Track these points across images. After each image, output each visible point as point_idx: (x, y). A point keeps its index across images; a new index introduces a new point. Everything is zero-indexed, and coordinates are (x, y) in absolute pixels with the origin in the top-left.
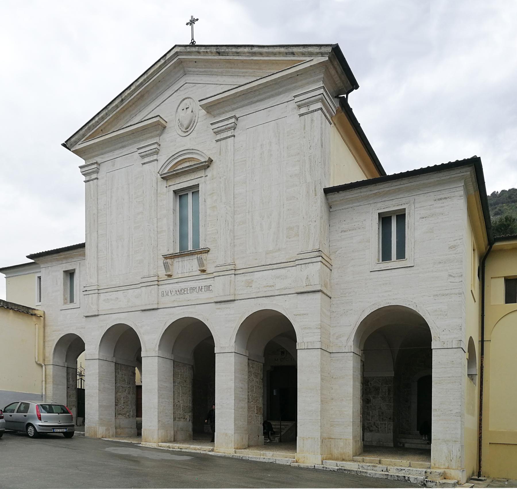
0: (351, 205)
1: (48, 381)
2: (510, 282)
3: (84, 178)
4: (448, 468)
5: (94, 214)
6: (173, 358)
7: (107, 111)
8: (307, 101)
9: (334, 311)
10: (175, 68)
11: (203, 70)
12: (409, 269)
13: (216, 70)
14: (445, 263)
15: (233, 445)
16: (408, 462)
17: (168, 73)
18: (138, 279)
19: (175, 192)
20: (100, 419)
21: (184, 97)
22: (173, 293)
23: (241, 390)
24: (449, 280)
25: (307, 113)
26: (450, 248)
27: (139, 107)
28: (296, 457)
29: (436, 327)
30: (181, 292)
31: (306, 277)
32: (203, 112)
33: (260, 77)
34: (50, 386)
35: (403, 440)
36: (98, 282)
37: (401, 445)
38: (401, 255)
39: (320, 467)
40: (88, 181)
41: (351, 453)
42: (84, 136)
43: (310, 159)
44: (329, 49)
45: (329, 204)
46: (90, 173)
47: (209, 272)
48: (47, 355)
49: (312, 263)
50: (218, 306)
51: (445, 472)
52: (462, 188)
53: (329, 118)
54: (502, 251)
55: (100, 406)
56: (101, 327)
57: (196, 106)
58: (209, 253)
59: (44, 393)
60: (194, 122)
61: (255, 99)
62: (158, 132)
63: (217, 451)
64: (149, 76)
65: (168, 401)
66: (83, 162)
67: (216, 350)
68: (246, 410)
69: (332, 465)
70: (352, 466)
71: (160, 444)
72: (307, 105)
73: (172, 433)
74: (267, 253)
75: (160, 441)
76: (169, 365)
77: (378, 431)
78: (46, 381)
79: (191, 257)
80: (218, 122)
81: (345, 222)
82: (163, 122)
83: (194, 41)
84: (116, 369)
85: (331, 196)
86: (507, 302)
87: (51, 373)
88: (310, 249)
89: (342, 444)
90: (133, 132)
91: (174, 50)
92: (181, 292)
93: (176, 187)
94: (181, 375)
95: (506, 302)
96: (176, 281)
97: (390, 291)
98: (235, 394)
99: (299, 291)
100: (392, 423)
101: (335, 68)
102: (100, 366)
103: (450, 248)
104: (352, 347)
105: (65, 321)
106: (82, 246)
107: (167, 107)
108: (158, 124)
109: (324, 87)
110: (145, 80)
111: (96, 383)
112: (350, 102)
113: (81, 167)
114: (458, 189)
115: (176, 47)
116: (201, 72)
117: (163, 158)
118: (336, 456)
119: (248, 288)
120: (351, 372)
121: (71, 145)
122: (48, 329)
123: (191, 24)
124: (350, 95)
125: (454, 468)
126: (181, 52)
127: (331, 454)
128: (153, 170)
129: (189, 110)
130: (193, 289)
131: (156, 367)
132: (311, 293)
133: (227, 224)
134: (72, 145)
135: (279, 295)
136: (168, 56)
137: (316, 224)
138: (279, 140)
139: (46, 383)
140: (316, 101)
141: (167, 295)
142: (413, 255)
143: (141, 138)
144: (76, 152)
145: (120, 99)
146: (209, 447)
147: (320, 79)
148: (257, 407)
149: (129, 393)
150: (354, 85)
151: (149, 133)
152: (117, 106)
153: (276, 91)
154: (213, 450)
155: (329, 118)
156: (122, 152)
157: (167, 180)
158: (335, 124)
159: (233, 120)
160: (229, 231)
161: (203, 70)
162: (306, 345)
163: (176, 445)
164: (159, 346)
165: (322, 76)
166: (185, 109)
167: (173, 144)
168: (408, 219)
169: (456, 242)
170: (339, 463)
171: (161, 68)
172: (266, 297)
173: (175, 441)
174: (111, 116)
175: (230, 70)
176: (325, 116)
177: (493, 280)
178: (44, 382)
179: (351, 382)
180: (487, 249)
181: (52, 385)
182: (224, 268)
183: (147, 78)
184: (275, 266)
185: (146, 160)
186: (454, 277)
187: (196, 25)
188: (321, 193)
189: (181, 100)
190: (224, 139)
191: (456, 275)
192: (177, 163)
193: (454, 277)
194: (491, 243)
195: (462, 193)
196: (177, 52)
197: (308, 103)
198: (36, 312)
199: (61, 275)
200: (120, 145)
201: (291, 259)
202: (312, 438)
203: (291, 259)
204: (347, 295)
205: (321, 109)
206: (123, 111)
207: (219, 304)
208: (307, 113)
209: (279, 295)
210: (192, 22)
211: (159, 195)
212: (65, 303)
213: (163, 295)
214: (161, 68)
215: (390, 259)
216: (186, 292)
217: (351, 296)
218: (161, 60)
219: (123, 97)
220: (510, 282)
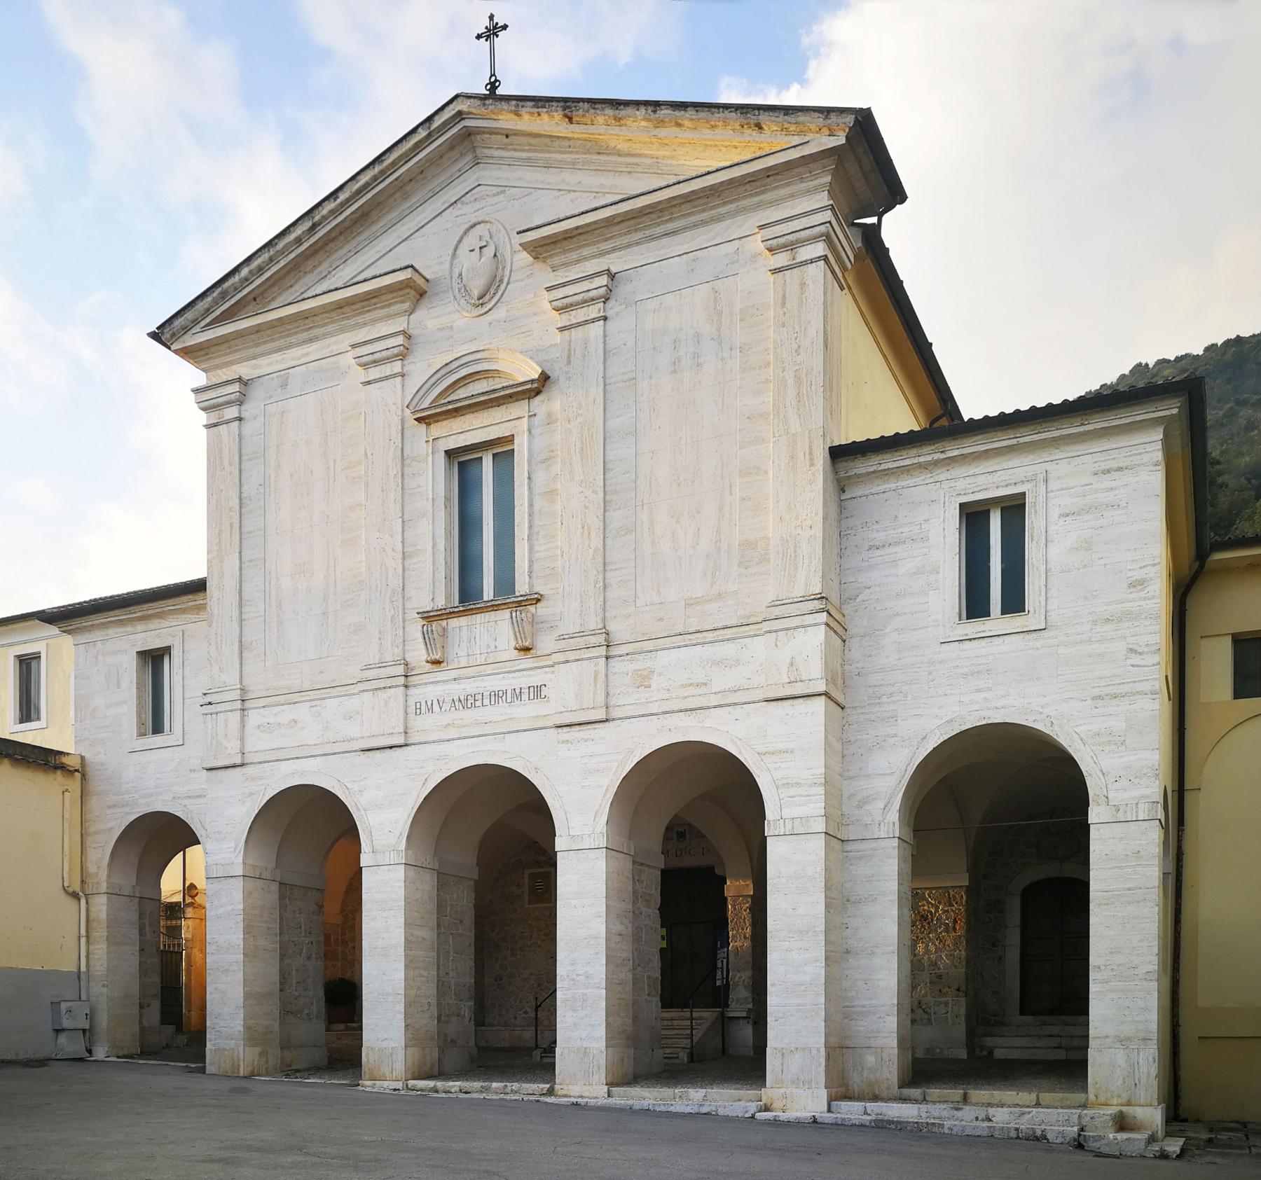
0: (893, 486)
1: (95, 934)
2: (1242, 643)
3: (203, 418)
4: (1129, 1104)
5: (231, 509)
6: (437, 867)
7: (272, 252)
8: (790, 237)
9: (853, 739)
10: (452, 148)
11: (525, 155)
12: (1034, 635)
13: (559, 156)
14: (1119, 621)
15: (603, 1075)
16: (1034, 1096)
17: (435, 161)
18: (354, 672)
19: (449, 453)
20: (247, 1028)
21: (474, 221)
22: (446, 707)
23: (619, 939)
24: (1130, 662)
25: (789, 268)
26: (1131, 585)
27: (354, 242)
28: (764, 1098)
29: (1100, 774)
30: (466, 702)
31: (788, 662)
32: (525, 257)
33: (674, 179)
34: (101, 949)
35: (989, 1041)
36: (241, 682)
37: (985, 1053)
38: (1014, 602)
39: (828, 1118)
40: (215, 425)
41: (896, 1080)
42: (208, 311)
43: (798, 379)
44: (850, 120)
45: (839, 481)
46: (224, 405)
47: (539, 653)
48: (92, 869)
49: (803, 627)
50: (565, 734)
51: (1121, 1112)
52: (1159, 446)
53: (840, 275)
54: (1228, 570)
55: (247, 996)
56: (251, 794)
57: (511, 245)
58: (539, 605)
59: (83, 969)
60: (501, 281)
61: (659, 230)
62: (406, 306)
63: (563, 1092)
64: (387, 168)
65: (425, 974)
66: (199, 378)
67: (560, 844)
68: (629, 988)
69: (851, 1111)
70: (895, 1111)
71: (411, 1083)
72: (791, 247)
73: (436, 1055)
74: (687, 605)
75: (409, 1075)
76: (428, 882)
77: (930, 1022)
78: (88, 937)
79: (491, 616)
80: (564, 285)
81: (876, 527)
82: (420, 281)
83: (496, 80)
84: (282, 898)
85: (845, 464)
86: (1238, 695)
87: (103, 916)
88: (799, 591)
89: (871, 1059)
90: (340, 306)
91: (451, 106)
92: (466, 702)
93: (453, 444)
94: (452, 906)
95: (1236, 697)
96: (453, 674)
97: (990, 689)
98: (607, 949)
99: (772, 695)
100: (963, 1000)
101: (859, 161)
102: (247, 895)
103: (1131, 585)
104: (897, 824)
105: (149, 777)
106: (198, 587)
107: (422, 240)
108: (407, 285)
109: (833, 209)
110: (375, 178)
111: (237, 938)
112: (885, 235)
113: (197, 391)
114: (1149, 448)
115: (460, 99)
116: (519, 159)
117: (421, 368)
118: (856, 1090)
119: (642, 689)
120: (894, 885)
121: (173, 335)
122: (94, 803)
123: (488, 37)
124: (886, 218)
125: (1142, 1102)
126: (469, 113)
127: (846, 1085)
128: (389, 401)
129: (489, 252)
130: (497, 696)
131: (401, 893)
132: (801, 700)
133: (586, 534)
134: (175, 336)
135: (720, 706)
136: (437, 122)
137: (812, 532)
138: (719, 330)
139: (88, 942)
140: (814, 239)
141: (431, 710)
142: (1043, 603)
143: (360, 319)
144: (186, 353)
145: (307, 224)
146: (542, 1086)
147: (823, 185)
148: (649, 977)
149: (309, 958)
150: (894, 194)
151: (382, 307)
152: (299, 241)
153: (713, 212)
154: (551, 1092)
155: (840, 275)
156: (307, 354)
157: (428, 424)
158: (849, 288)
159: (604, 280)
160: (591, 552)
161: (525, 155)
162: (789, 826)
163: (451, 1083)
164: (408, 837)
165: (828, 179)
166: (477, 249)
167: (448, 334)
168: (1034, 522)
169: (1146, 570)
170: (871, 1106)
171: (418, 147)
172: (686, 710)
173: (441, 1075)
174: (282, 263)
175: (594, 157)
176: (833, 272)
177: (1204, 641)
178: (83, 940)
179: (895, 912)
180: (1194, 570)
181: (104, 946)
182: (581, 642)
183: (382, 172)
184: (710, 636)
185: (375, 373)
186: (1140, 654)
187: (502, 39)
188: (821, 457)
189: (467, 226)
190: (579, 325)
191: (1146, 650)
192: (455, 383)
193: (1140, 654)
194: (1201, 555)
195: (1159, 456)
196: (460, 113)
197: (792, 243)
198: (65, 760)
199: (129, 665)
200: (305, 335)
201: (749, 617)
202: (803, 1049)
203: (749, 617)
204: (884, 699)
205: (825, 258)
206: (314, 251)
207: (565, 729)
208: (789, 268)
209: (720, 706)
210: (493, 31)
211: (407, 462)
212: (142, 734)
213: (418, 711)
214: (418, 147)
215: (986, 613)
216: (478, 704)
217: (894, 703)
218: (420, 130)
219: (317, 219)
220: (1242, 643)
